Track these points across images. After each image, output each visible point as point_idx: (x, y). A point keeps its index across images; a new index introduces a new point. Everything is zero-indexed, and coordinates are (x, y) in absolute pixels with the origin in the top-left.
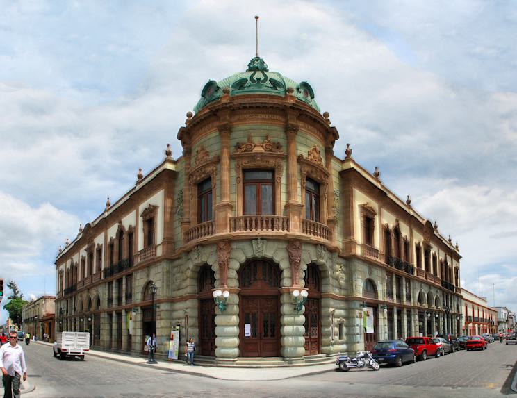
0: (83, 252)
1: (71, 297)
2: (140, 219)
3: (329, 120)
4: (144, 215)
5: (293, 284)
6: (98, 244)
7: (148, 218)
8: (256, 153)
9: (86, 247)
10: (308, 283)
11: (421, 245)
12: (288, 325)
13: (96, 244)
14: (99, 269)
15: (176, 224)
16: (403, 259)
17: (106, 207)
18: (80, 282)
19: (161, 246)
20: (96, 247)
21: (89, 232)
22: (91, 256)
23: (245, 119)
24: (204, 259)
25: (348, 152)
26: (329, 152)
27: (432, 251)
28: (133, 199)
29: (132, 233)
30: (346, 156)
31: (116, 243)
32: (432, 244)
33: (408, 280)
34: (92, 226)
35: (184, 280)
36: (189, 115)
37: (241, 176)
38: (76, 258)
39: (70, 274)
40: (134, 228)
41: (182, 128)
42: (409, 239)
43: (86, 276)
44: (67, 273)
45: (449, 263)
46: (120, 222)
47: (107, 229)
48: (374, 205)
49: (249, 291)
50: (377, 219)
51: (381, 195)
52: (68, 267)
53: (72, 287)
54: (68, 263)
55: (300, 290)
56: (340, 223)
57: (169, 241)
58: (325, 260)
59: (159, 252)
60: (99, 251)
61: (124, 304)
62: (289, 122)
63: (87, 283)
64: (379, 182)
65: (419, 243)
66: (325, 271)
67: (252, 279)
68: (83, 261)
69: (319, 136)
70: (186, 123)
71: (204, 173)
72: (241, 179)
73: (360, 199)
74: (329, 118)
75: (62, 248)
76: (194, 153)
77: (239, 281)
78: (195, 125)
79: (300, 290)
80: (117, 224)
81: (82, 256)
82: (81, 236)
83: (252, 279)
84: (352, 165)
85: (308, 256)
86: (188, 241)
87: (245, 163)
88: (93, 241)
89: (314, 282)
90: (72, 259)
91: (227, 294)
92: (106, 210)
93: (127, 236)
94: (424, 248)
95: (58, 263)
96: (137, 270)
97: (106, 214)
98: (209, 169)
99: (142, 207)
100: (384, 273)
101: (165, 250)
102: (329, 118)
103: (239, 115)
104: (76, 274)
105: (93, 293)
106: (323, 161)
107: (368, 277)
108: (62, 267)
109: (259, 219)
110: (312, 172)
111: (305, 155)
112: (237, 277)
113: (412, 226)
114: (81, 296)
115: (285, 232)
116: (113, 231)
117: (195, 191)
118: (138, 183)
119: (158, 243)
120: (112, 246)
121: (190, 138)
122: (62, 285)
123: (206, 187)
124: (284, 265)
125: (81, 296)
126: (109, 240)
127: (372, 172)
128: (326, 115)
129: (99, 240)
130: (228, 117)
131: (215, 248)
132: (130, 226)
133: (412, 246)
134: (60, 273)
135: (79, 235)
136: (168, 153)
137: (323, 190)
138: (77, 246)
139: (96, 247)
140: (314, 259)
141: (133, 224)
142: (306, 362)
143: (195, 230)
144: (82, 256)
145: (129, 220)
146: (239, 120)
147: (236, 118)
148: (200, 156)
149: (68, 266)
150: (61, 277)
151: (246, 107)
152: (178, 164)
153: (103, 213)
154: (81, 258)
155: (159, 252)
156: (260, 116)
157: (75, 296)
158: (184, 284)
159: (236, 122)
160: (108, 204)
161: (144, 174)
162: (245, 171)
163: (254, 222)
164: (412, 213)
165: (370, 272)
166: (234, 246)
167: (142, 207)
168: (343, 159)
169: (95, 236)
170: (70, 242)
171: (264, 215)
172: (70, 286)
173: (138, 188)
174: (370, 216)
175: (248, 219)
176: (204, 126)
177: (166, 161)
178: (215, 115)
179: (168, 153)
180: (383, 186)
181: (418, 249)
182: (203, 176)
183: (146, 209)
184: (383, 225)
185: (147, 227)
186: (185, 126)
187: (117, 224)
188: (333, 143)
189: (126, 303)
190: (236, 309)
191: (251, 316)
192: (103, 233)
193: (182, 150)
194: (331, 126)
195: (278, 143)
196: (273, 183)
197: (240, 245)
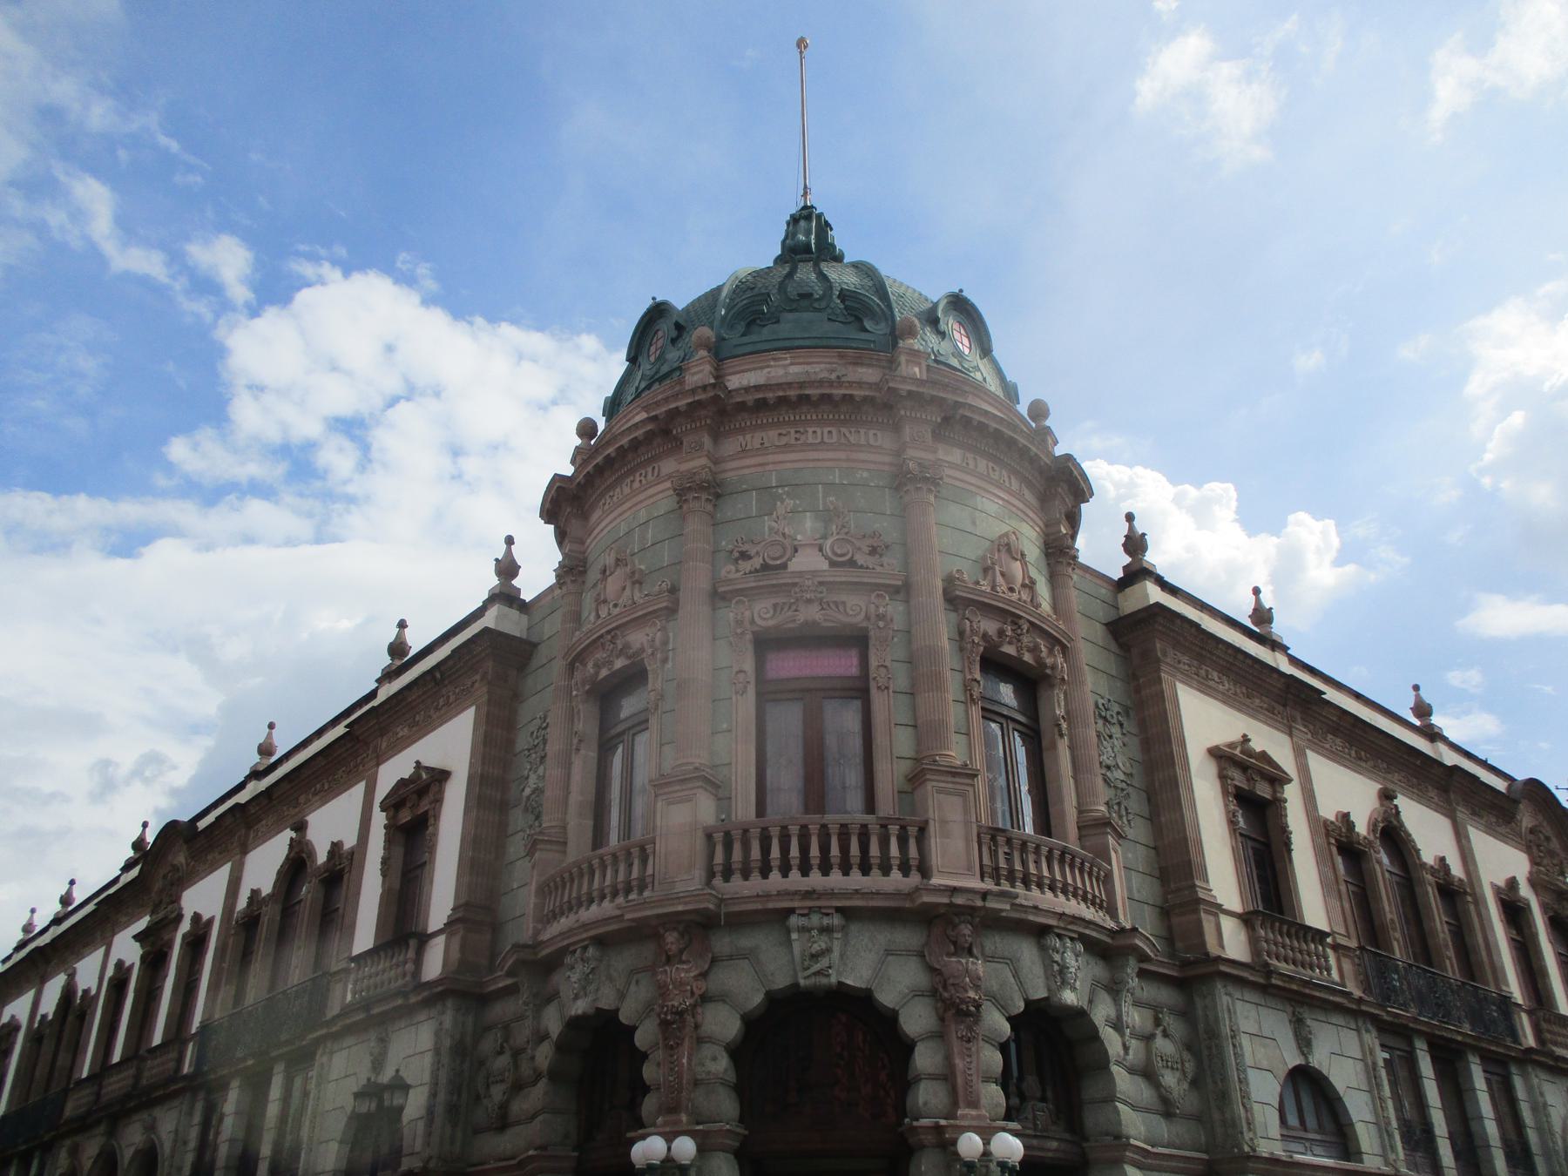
0: (126, 947)
2: (379, 819)
3: (1048, 431)
4: (394, 804)
5: (955, 1104)
7: (405, 816)
8: (801, 574)
9: (142, 924)
10: (1023, 1097)
11: (1525, 891)
15: (516, 847)
16: (1452, 969)
17: (256, 758)
18: (81, 1082)
19: (431, 930)
20: (185, 926)
21: (171, 855)
22: (154, 961)
24: (607, 1001)
25: (1135, 544)
26: (1059, 552)
28: (363, 734)
30: (1128, 560)
31: (270, 915)
33: (1499, 1068)
35: (518, 1087)
36: (587, 428)
37: (749, 665)
38: (89, 972)
40: (352, 853)
41: (557, 478)
42: (1457, 870)
43: (116, 1057)
46: (301, 827)
47: (245, 851)
50: (1292, 794)
51: (1297, 700)
52: (42, 1010)
55: (987, 1134)
56: (1138, 830)
57: (477, 913)
59: (434, 964)
60: (196, 942)
62: (911, 453)
63: (115, 1086)
64: (1276, 645)
66: (1094, 1036)
68: (118, 985)
69: (1021, 498)
70: (573, 462)
71: (621, 653)
72: (752, 679)
73: (1205, 721)
74: (1048, 423)
75: (41, 922)
76: (593, 575)
78: (600, 470)
79: (987, 1134)
80: (288, 834)
81: (120, 964)
82: (135, 872)
84: (1155, 594)
85: (1007, 978)
86: (554, 916)
87: (763, 613)
88: (176, 900)
89: (1049, 1094)
91: (685, 1147)
92: (256, 774)
93: (316, 887)
94: (1545, 907)
96: (336, 1037)
97: (254, 788)
98: (637, 638)
99: (394, 771)
100: (1372, 1039)
101: (455, 955)
102: (1048, 423)
103: (742, 430)
105: (132, 1138)
106: (1043, 589)
107: (1293, 1060)
109: (814, 829)
110: (1001, 633)
112: (731, 1077)
113: (1462, 814)
115: (915, 879)
116: (264, 865)
117: (587, 724)
118: (388, 675)
119: (441, 939)
121: (585, 516)
123: (629, 706)
124: (916, 1020)
125: (74, 1152)
126: (242, 903)
127: (1242, 610)
128: (1039, 410)
129: (204, 898)
130: (707, 440)
131: (648, 951)
132: (336, 847)
133: (1479, 901)
135: (127, 867)
136: (507, 569)
137: (1056, 705)
138: (110, 908)
139: (185, 926)
140: (1040, 993)
141: (350, 841)
143: (581, 875)
144: (120, 964)
145: (335, 822)
147: (730, 446)
148: (612, 585)
149: (50, 1003)
154: (110, 972)
155: (434, 964)
158: (519, 1106)
159: (733, 458)
160: (265, 750)
161: (416, 643)
162: (765, 644)
164: (1450, 758)
165: (1304, 1043)
166: (722, 943)
167: (394, 771)
168: (1117, 574)
170: (79, 896)
171: (833, 819)
173: (382, 696)
174: (1263, 790)
175: (775, 832)
176: (632, 472)
177: (494, 598)
178: (666, 432)
179: (507, 569)
180: (1294, 661)
181: (1514, 911)
182: (619, 664)
183: (402, 783)
184: (1326, 823)
185: (399, 851)
186: (568, 470)
187: (288, 834)
188: (1073, 520)
192: (227, 868)
193: (558, 557)
194: (1059, 451)
197: (746, 941)
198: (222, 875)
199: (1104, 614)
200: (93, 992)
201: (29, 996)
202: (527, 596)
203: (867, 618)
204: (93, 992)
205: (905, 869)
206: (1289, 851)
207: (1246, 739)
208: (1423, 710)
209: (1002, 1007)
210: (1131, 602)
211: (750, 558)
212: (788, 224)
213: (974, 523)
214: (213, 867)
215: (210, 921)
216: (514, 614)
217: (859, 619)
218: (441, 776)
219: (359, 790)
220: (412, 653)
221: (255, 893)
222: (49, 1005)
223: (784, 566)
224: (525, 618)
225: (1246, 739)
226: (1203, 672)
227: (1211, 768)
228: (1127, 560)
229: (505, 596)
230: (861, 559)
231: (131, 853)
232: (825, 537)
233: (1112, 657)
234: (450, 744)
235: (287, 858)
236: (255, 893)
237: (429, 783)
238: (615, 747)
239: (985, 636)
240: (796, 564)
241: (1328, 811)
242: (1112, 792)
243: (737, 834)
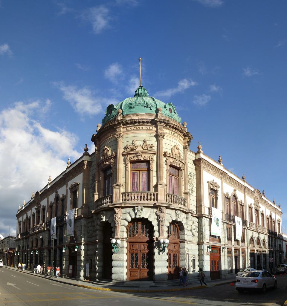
0: (34, 210)
1: (26, 238)
2: (69, 191)
4: (71, 188)
6: (43, 206)
13: (42, 205)
19: (80, 209)
20: (42, 207)
22: (38, 212)
27: (261, 210)
29: (64, 199)
32: (260, 205)
34: (40, 193)
38: (29, 214)
39: (26, 224)
42: (243, 202)
44: (24, 223)
45: (273, 217)
46: (57, 192)
48: (218, 181)
49: (133, 239)
52: (24, 219)
53: (26, 232)
54: (25, 216)
58: (182, 218)
60: (44, 209)
61: (58, 245)
65: (251, 204)
67: (135, 232)
68: (34, 215)
80: (55, 193)
81: (33, 213)
83: (135, 232)
89: (175, 233)
90: (27, 214)
99: (71, 183)
104: (30, 224)
108: (21, 219)
111: (169, 151)
114: (32, 238)
116: (52, 198)
120: (51, 207)
124: (155, 223)
126: (49, 204)
129: (44, 203)
134: (19, 223)
139: (42, 207)
140: (174, 219)
144: (33, 213)
145: (62, 191)
150: (20, 225)
152: (92, 157)
153: (31, 200)
154: (32, 214)
157: (28, 237)
169: (42, 200)
172: (25, 231)
173: (68, 171)
174: (215, 188)
179: (86, 150)
181: (250, 208)
185: (72, 196)
187: (55, 193)
189: (60, 244)
190: (125, 251)
191: (134, 255)
192: (22, 217)
198: (46, 199)
202: (90, 154)
205: (154, 200)
206: (218, 198)
209: (168, 221)
211: (129, 148)
215: (45, 206)
226: (208, 169)
229: (86, 154)
235: (55, 197)
236: (51, 202)
238: (106, 179)
241: (225, 192)
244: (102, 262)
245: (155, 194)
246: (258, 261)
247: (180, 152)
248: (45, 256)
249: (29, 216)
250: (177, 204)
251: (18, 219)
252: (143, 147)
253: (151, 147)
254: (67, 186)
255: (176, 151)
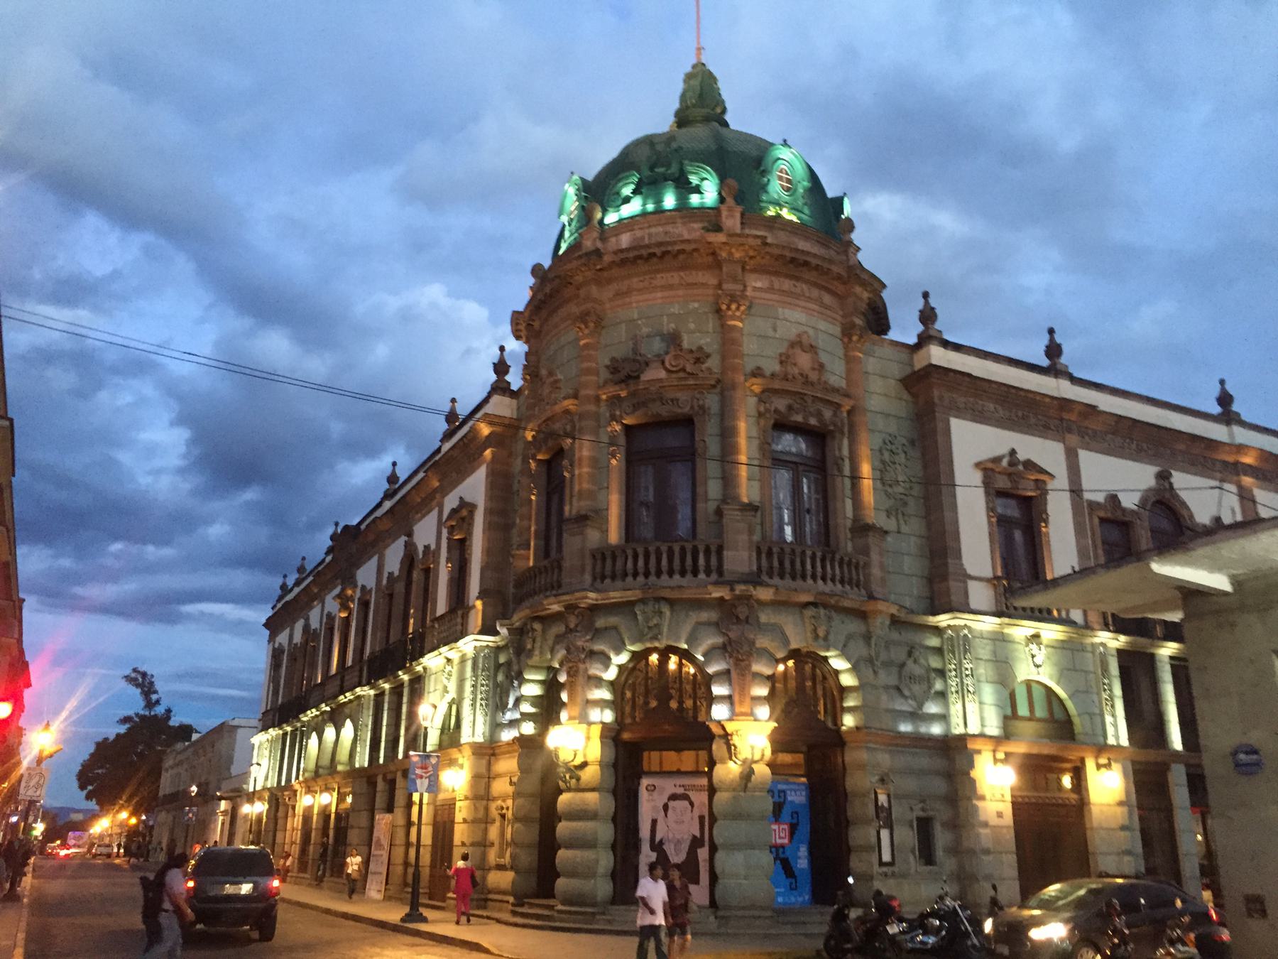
6: (363, 587)
12: (570, 846)
14: (360, 650)
17: (387, 486)
23: (628, 293)
31: (400, 588)
38: (315, 618)
40: (434, 553)
46: (410, 534)
60: (365, 604)
77: (682, 750)
80: (404, 538)
90: (307, 619)
95: (273, 625)
97: (388, 505)
99: (451, 502)
108: (283, 638)
110: (790, 408)
116: (394, 556)
118: (448, 436)
122: (276, 692)
132: (427, 548)
134: (276, 655)
136: (501, 368)
142: (514, 913)
146: (618, 294)
151: (654, 254)
153: (379, 505)
156: (661, 279)
163: (665, 557)
167: (451, 502)
168: (912, 340)
173: (447, 446)
184: (1093, 505)
192: (375, 559)
195: (700, 349)
196: (690, 455)
198: (373, 562)
199: (897, 371)
200: (433, 547)
201: (287, 631)
203: (692, 407)
204: (433, 547)
207: (1013, 452)
208: (1225, 399)
210: (919, 362)
212: (685, 81)
213: (775, 330)
214: (283, 629)
215: (370, 591)
216: (507, 400)
217: (686, 410)
218: (472, 508)
219: (435, 513)
220: (401, 481)
221: (391, 574)
222: (298, 638)
223: (638, 377)
224: (514, 402)
225: (1013, 452)
227: (977, 477)
228: (921, 328)
230: (689, 368)
231: (330, 543)
232: (667, 353)
233: (904, 403)
234: (475, 487)
236: (391, 574)
237: (466, 508)
239: (776, 411)
240: (648, 375)
242: (891, 502)
243: (608, 554)
244: (851, 843)
245: (713, 548)
246: (679, 902)
247: (824, 358)
248: (255, 888)
249: (315, 630)
250: (810, 581)
251: (272, 639)
252: (667, 365)
253: (698, 361)
254: (441, 513)
255: (804, 360)
